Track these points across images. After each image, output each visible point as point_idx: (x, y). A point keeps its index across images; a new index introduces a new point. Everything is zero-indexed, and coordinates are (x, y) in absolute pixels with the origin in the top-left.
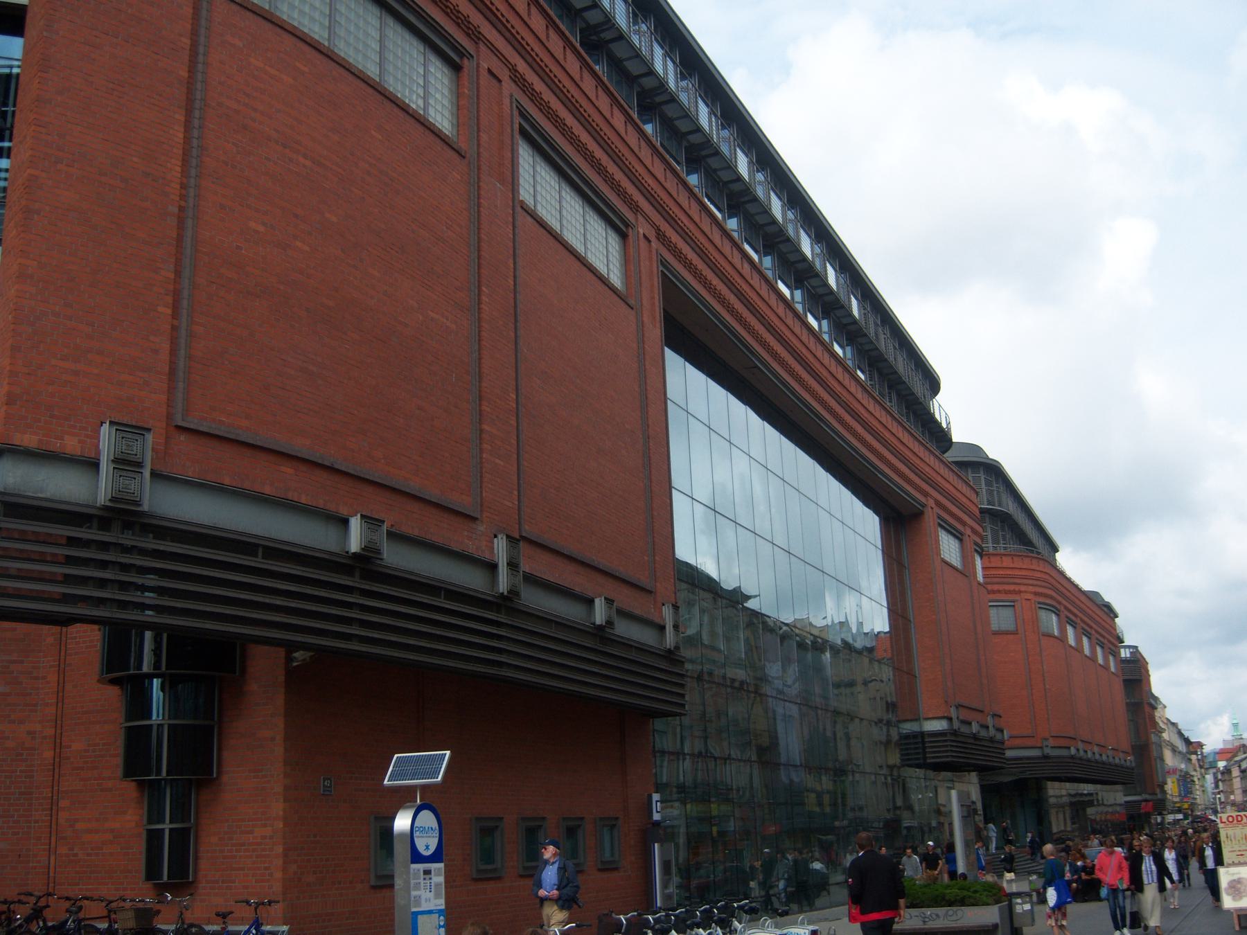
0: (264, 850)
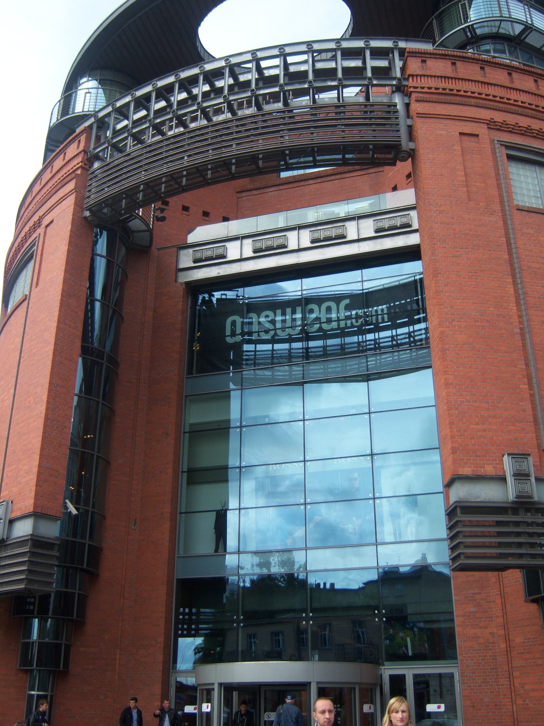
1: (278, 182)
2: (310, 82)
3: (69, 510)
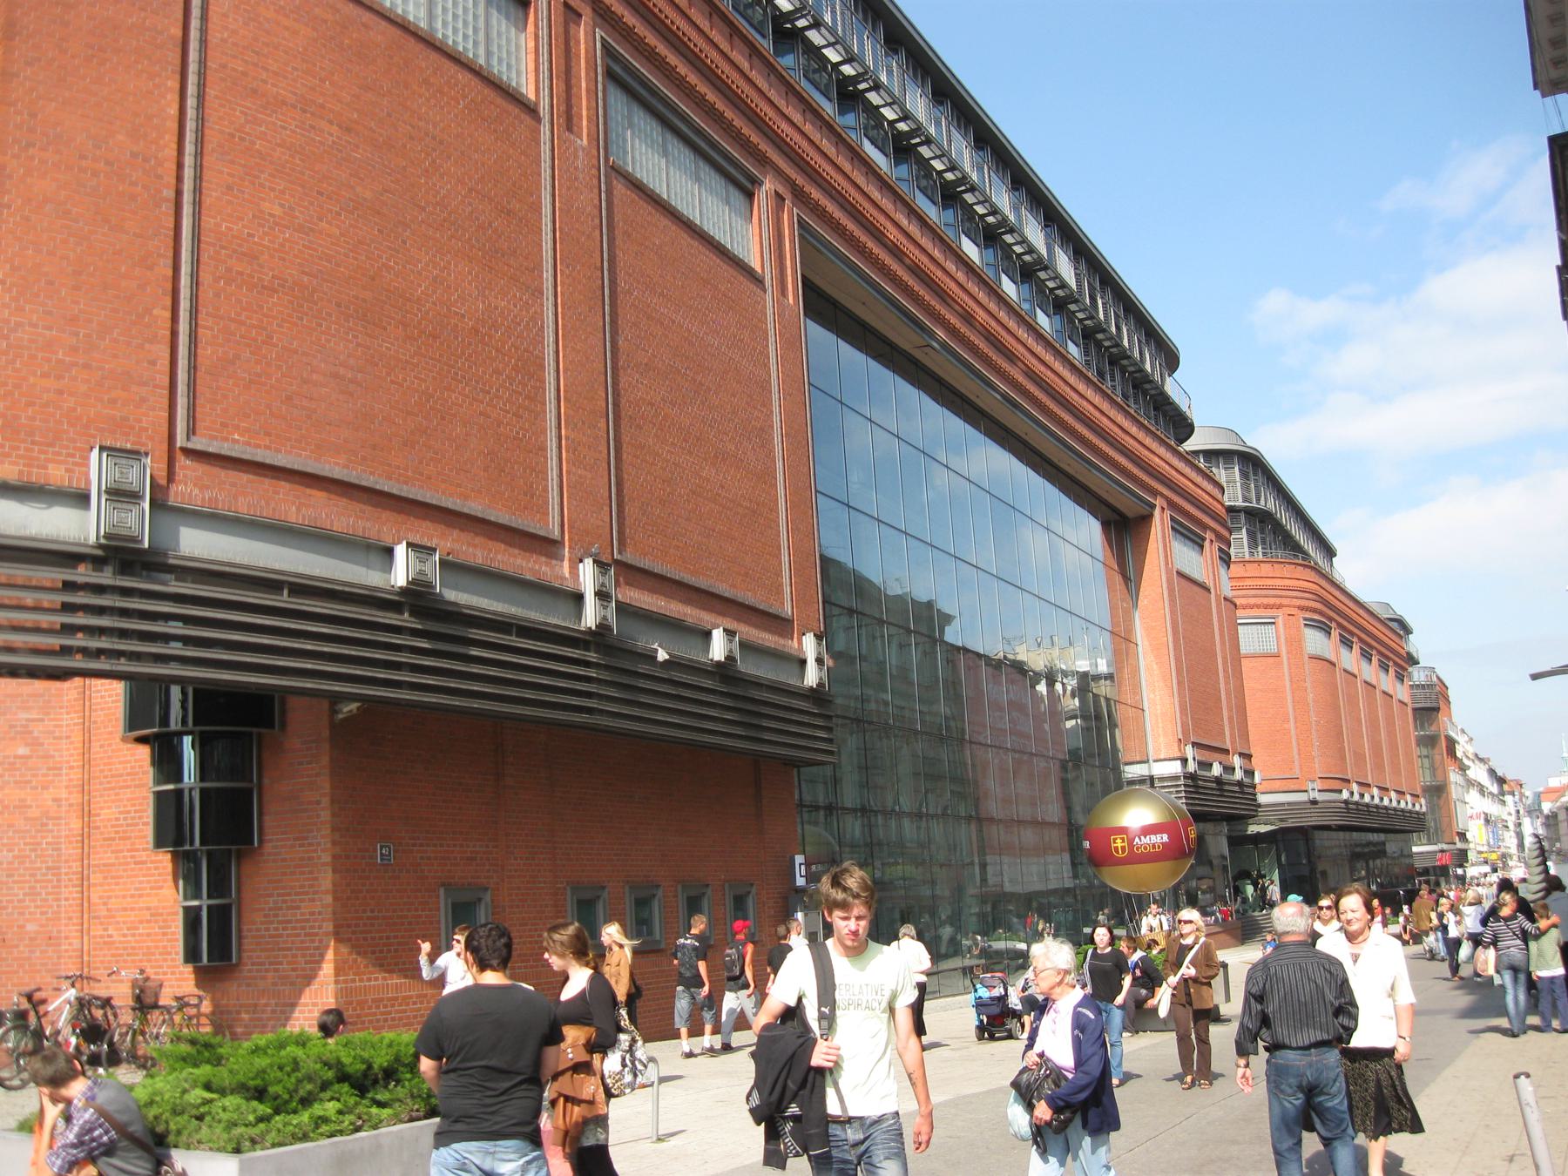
0: (311, 927)
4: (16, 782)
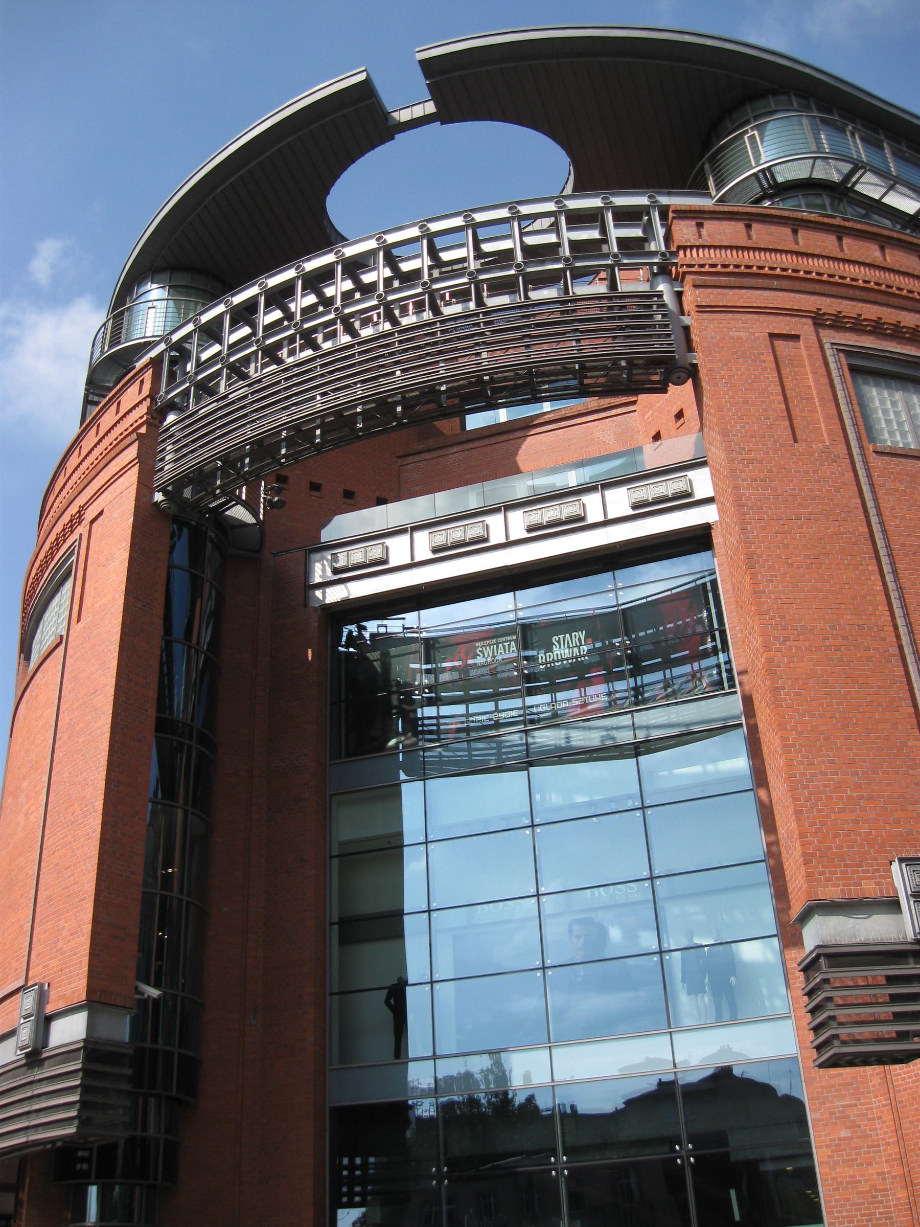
1: (464, 438)
2: (518, 266)
3: (146, 995)
4: (844, 1161)
